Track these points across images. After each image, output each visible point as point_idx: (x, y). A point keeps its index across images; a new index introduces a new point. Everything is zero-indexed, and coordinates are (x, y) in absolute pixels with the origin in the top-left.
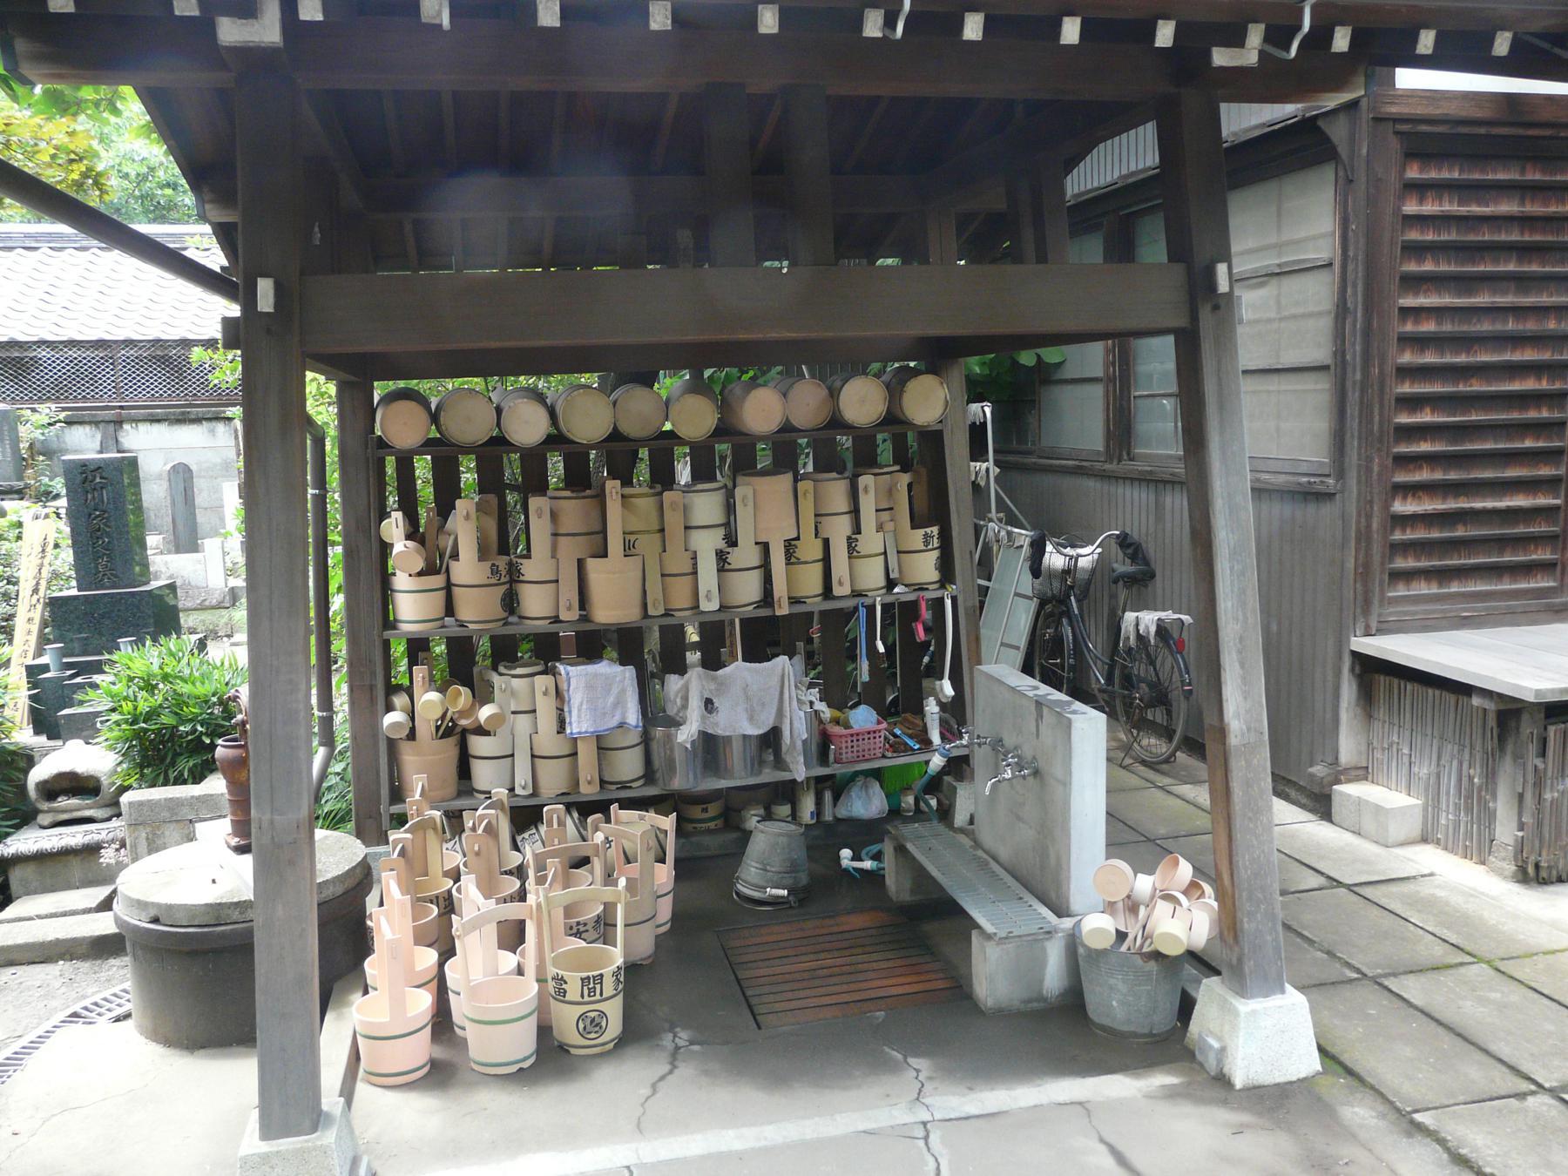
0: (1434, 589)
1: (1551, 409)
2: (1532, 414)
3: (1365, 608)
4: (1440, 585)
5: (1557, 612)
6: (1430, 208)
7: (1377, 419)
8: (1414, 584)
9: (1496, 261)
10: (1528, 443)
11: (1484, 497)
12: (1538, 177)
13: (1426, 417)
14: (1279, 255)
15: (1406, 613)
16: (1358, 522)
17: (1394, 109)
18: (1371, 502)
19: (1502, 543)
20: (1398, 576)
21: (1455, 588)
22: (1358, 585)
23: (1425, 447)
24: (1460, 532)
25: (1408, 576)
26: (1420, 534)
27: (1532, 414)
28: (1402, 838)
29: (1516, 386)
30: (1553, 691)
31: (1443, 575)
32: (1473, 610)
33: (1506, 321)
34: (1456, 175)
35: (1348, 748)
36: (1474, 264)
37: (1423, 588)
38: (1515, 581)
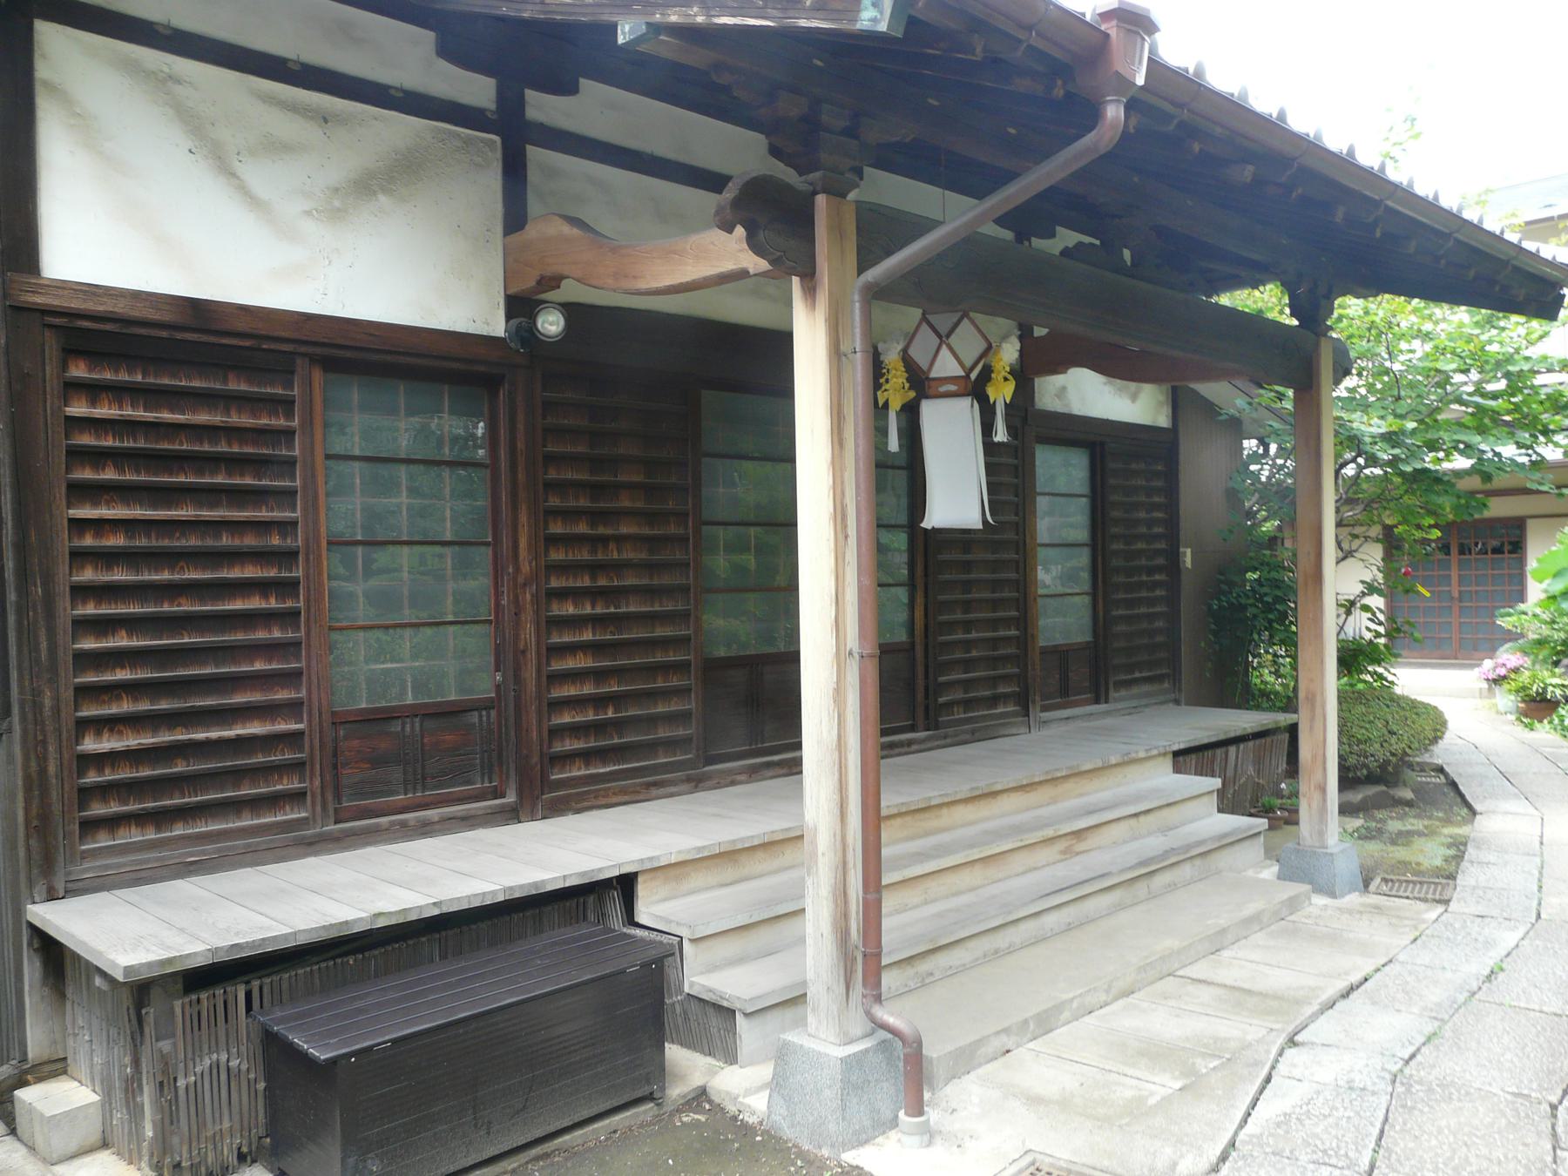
0: (151, 835)
1: (283, 628)
2: (261, 635)
3: (51, 871)
4: (159, 829)
5: (310, 844)
6: (104, 411)
7: (44, 645)
8: (122, 832)
9: (200, 473)
10: (259, 666)
11: (208, 727)
12: (243, 387)
13: (121, 641)
14: (966, 692)
15: (107, 867)
16: (26, 766)
17: (38, 299)
18: (44, 742)
19: (237, 775)
20: (90, 826)
21: (179, 830)
22: (33, 842)
23: (122, 675)
24: (180, 767)
25: (113, 823)
26: (124, 774)
27: (261, 635)
28: (73, 1147)
29: (238, 605)
30: (150, 965)
31: (160, 818)
32: (203, 853)
33: (218, 536)
34: (139, 378)
35: (36, 1040)
36: (171, 474)
37: (134, 835)
38: (259, 816)
